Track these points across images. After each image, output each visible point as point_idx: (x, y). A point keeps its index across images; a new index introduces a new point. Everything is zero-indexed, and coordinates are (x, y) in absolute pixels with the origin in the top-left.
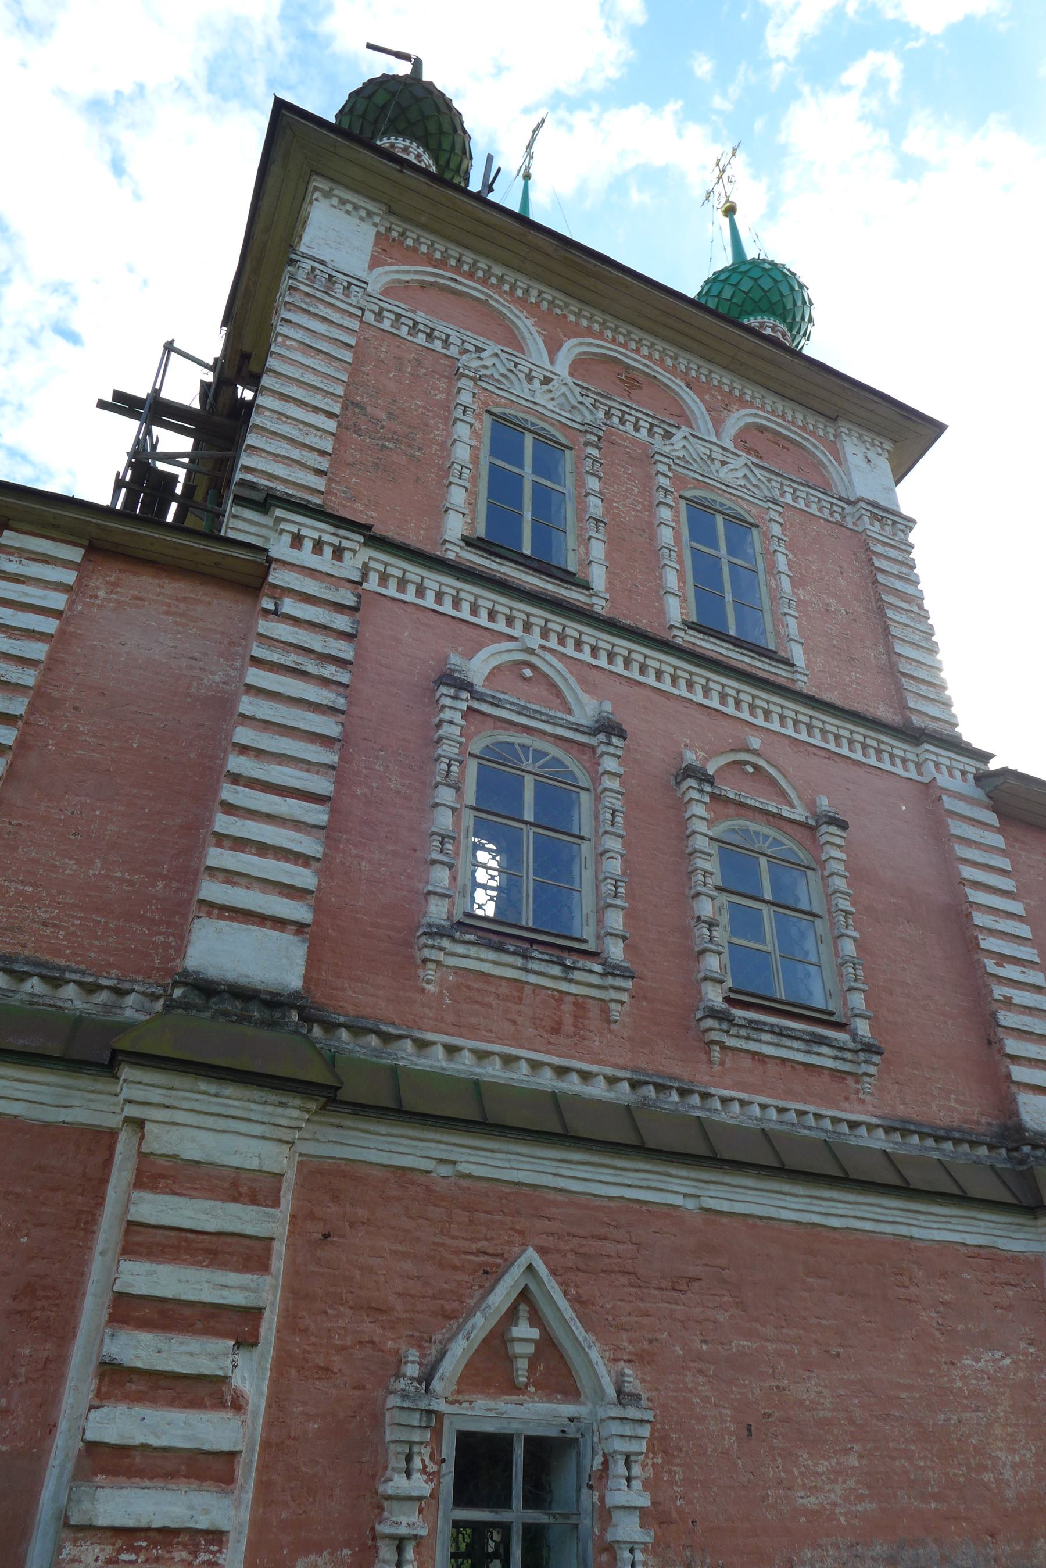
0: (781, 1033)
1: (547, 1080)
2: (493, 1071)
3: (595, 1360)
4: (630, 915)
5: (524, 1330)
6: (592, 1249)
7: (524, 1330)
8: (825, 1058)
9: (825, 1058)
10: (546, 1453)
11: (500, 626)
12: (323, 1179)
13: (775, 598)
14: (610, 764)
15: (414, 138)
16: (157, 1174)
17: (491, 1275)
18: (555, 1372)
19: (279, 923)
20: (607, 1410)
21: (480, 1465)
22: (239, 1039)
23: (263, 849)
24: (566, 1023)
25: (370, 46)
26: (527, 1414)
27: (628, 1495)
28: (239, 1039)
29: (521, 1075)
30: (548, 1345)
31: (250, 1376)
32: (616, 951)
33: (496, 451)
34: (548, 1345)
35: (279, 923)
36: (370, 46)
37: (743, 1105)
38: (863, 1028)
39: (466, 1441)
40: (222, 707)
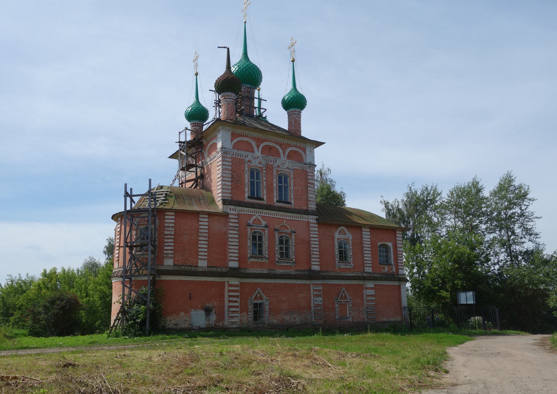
0: (284, 262)
1: (260, 272)
2: (255, 272)
3: (264, 297)
4: (268, 252)
5: (259, 295)
6: (264, 287)
7: (259, 295)
8: (289, 264)
9: (289, 264)
10: (261, 304)
11: (253, 214)
12: (242, 284)
13: (290, 189)
14: (266, 232)
15: (293, 107)
16: (230, 286)
17: (256, 290)
18: (261, 298)
19: (235, 260)
20: (265, 301)
21: (256, 305)
22: (234, 273)
23: (233, 253)
24: (261, 265)
25: (150, 180)
26: (259, 301)
27: (267, 307)
28: (234, 273)
29: (257, 272)
30: (261, 296)
31: (238, 300)
32: (267, 256)
33: (251, 178)
34: (261, 296)
35: (235, 260)
36: (150, 180)
37: (279, 271)
38: (294, 260)
39: (254, 304)
40: (226, 233)
